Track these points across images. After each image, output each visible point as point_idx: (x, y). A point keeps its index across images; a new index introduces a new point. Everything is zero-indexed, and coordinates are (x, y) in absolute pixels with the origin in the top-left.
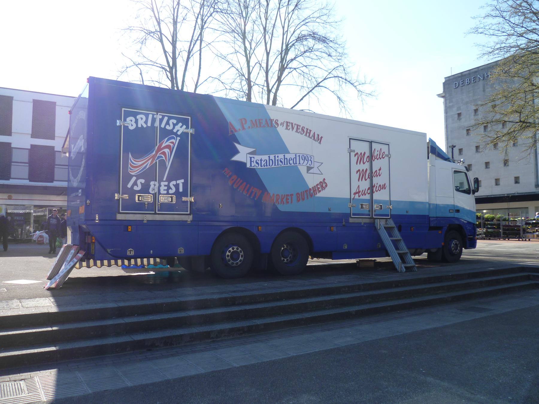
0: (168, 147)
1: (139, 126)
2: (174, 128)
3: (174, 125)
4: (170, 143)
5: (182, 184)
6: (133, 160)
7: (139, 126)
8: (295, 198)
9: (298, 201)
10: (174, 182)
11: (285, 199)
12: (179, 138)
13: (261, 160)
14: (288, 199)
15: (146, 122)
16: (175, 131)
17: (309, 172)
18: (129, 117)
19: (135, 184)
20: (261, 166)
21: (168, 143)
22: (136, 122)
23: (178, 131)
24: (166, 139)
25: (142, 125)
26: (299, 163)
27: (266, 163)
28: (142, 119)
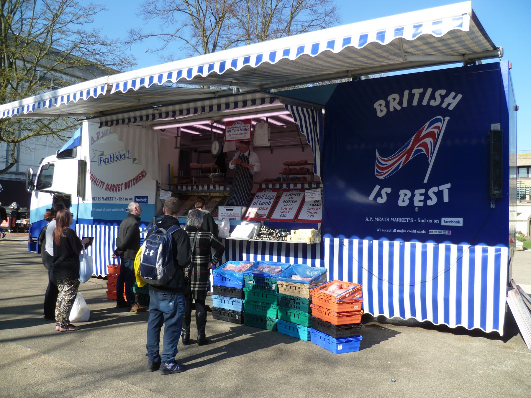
0: (431, 135)
1: (392, 109)
2: (442, 102)
3: (443, 97)
4: (433, 128)
5: (447, 190)
8: (123, 186)
9: (126, 188)
10: (435, 189)
11: (118, 187)
12: (447, 119)
13: (106, 159)
15: (400, 103)
16: (444, 106)
18: (378, 100)
19: (379, 194)
20: (106, 163)
21: (430, 130)
22: (387, 106)
23: (449, 104)
25: (394, 108)
26: (128, 157)
27: (109, 160)
28: (394, 99)
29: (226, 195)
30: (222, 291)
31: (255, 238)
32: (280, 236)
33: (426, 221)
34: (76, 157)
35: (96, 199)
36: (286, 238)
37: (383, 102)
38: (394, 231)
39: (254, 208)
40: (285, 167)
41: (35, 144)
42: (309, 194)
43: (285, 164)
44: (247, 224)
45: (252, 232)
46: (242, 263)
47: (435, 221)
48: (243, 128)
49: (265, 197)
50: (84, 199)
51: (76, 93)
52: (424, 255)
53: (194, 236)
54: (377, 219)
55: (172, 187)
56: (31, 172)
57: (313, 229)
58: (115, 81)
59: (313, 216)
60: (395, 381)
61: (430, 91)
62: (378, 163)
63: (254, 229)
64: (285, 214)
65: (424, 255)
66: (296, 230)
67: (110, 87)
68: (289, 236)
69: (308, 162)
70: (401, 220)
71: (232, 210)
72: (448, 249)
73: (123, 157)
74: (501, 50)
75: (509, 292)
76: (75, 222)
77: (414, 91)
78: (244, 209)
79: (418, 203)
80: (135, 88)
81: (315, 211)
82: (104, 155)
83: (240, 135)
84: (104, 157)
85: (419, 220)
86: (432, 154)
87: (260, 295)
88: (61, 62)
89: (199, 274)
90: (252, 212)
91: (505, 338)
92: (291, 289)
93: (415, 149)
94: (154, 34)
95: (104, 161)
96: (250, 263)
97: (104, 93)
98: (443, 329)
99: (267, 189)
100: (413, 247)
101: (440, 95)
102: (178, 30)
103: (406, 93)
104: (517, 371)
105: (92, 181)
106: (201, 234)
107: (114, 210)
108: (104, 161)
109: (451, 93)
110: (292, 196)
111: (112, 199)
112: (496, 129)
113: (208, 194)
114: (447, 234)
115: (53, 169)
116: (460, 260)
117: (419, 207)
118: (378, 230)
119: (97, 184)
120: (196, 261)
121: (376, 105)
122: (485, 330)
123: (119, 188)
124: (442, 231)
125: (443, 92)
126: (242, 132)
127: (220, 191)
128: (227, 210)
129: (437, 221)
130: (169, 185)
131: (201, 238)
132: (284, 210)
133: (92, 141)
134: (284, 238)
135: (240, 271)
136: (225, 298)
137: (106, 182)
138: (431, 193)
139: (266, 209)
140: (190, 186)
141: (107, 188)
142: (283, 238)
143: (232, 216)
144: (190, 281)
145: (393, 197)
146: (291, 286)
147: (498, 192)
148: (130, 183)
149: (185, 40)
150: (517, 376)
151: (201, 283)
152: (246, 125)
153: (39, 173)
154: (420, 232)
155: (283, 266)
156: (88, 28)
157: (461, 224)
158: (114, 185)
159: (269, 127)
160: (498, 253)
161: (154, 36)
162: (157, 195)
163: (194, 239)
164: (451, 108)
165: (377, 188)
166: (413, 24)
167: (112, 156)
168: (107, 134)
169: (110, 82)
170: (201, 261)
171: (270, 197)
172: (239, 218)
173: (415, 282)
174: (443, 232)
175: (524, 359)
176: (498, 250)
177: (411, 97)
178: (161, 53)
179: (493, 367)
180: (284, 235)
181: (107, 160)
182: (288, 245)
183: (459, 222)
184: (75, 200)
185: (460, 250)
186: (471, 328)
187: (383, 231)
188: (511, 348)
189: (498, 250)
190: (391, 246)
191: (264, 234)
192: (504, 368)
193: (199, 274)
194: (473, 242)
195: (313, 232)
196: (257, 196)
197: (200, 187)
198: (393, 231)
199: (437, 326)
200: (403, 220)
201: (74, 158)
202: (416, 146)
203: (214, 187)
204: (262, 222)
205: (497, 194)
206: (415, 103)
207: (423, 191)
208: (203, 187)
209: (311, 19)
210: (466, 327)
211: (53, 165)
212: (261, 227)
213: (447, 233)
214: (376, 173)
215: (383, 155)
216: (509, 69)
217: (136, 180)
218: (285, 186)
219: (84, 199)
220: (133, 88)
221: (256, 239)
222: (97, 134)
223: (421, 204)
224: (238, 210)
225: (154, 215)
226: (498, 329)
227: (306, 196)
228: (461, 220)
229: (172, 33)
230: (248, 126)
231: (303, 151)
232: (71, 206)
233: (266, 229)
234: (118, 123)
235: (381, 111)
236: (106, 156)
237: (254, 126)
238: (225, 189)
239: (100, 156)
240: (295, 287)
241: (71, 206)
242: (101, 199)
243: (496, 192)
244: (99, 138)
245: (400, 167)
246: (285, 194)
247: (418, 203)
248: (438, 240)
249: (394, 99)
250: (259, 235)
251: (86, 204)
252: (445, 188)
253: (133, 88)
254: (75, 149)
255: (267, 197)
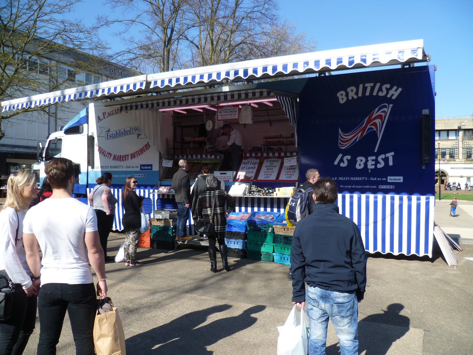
0: (380, 117)
1: (350, 98)
2: (387, 93)
3: (388, 90)
6: (343, 134)
7: (350, 98)
8: (130, 157)
9: (132, 158)
10: (383, 156)
11: (124, 157)
12: (391, 105)
13: (112, 134)
14: (126, 158)
15: (357, 93)
16: (389, 96)
17: (139, 138)
19: (341, 160)
20: (112, 138)
21: (379, 113)
22: (347, 95)
23: (393, 95)
24: (377, 109)
25: (352, 97)
26: (133, 133)
28: (352, 91)
29: (216, 162)
30: (228, 234)
31: (249, 195)
32: (268, 193)
33: (377, 179)
34: (83, 133)
35: (104, 167)
36: (273, 194)
37: (343, 93)
38: (354, 187)
39: (242, 172)
40: (265, 140)
41: (27, 121)
42: (287, 161)
43: (264, 138)
44: (239, 184)
45: (245, 190)
46: (241, 214)
47: (383, 179)
48: (233, 110)
49: (250, 163)
50: (93, 167)
51: (117, 87)
52: (376, 203)
53: (214, 194)
54: (341, 179)
55: (170, 156)
56: (41, 146)
57: (294, 187)
58: (153, 79)
59: (291, 177)
60: (369, 286)
61: (378, 85)
62: (341, 138)
63: (246, 188)
64: (268, 176)
65: (376, 203)
66: (280, 188)
67: (148, 83)
68: (275, 193)
69: (283, 136)
70: (358, 179)
71: (226, 174)
72: (392, 199)
73: (128, 133)
74: (429, 57)
75: (435, 227)
76: (86, 187)
77: (367, 85)
78: (235, 173)
79: (370, 166)
80: (171, 85)
81: (292, 173)
82: (110, 131)
83: (231, 116)
84: (110, 133)
85: (372, 179)
86: (380, 131)
87: (233, 243)
88: (44, 47)
89: (220, 221)
90: (241, 175)
91: (432, 260)
92: (284, 230)
93: (368, 127)
94: (119, 20)
95: (110, 136)
96: (248, 213)
97: (143, 88)
98: (389, 256)
99: (251, 156)
100: (368, 198)
101: (386, 88)
102: (139, 16)
103: (361, 86)
104: (445, 278)
105: (100, 153)
106: (209, 192)
107: (121, 176)
108: (110, 136)
109: (393, 87)
110: (272, 163)
111: (119, 167)
112: (425, 113)
113: (200, 161)
114: (392, 188)
115: (61, 143)
116: (401, 206)
117: (371, 169)
118: (341, 186)
119: (105, 155)
120: (217, 211)
121: (339, 95)
122: (419, 255)
123: (126, 158)
124: (388, 186)
125: (388, 86)
126: (232, 113)
127: (211, 159)
128: (221, 174)
129: (385, 179)
130: (168, 155)
131: (219, 194)
132: (267, 173)
133: (98, 120)
134: (271, 194)
135: (242, 219)
136: (231, 240)
137: (114, 153)
138: (380, 159)
139: (252, 172)
140: (186, 156)
141: (114, 158)
142: (270, 194)
143: (225, 179)
144: (214, 226)
145: (352, 162)
146: (284, 229)
147: (428, 158)
148: (136, 154)
149: (146, 25)
150: (445, 280)
151: (221, 227)
152: (234, 108)
153: (46, 146)
154: (372, 187)
155: (274, 215)
156: (69, 17)
157: (402, 181)
158: (121, 156)
159: (252, 109)
160: (428, 200)
161: (119, 22)
162: (160, 163)
163: (214, 196)
164: (394, 98)
165: (340, 156)
166: (385, 52)
167: (118, 132)
168: (112, 114)
169: (149, 80)
170: (220, 211)
171: (254, 164)
172: (231, 180)
173: (369, 223)
174: (388, 187)
175: (447, 271)
176: (428, 199)
177: (365, 89)
178: (123, 35)
179: (429, 276)
180: (271, 192)
181: (113, 136)
182: (272, 199)
183: (400, 179)
184: (84, 168)
185: (401, 199)
186: (409, 254)
187: (345, 187)
188: (437, 266)
189: (428, 199)
190: (351, 198)
191: (254, 191)
192: (435, 276)
193: (220, 221)
194: (410, 193)
195: (293, 188)
196: (243, 163)
197: (194, 156)
198: (353, 187)
199: (384, 255)
200: (360, 178)
201: (80, 133)
202: (369, 125)
203: (206, 156)
204: (251, 182)
205: (427, 159)
206: (368, 94)
207: (374, 158)
208: (197, 156)
209: (253, 6)
210: (406, 254)
211: (60, 140)
212: (250, 187)
213: (392, 187)
214: (339, 145)
215: (344, 132)
216: (435, 71)
217: (141, 152)
218: (265, 155)
219: (93, 167)
220: (170, 85)
221: (249, 196)
222: (103, 113)
223: (373, 167)
224: (230, 174)
225: (158, 179)
226: (428, 253)
227: (285, 162)
228: (401, 178)
229: (133, 19)
230: (236, 109)
231: (271, 126)
232: (81, 174)
233: (255, 188)
234: (137, 108)
235: (343, 99)
236: (113, 132)
237: (240, 109)
238: (216, 157)
239: (106, 132)
240: (288, 229)
241: (81, 174)
242: (109, 167)
243: (426, 158)
244: (105, 117)
245: (357, 140)
246: (266, 160)
247: (370, 166)
248: (386, 192)
249: (352, 91)
250: (250, 192)
251: (96, 172)
252: (390, 155)
253: (170, 85)
254: (81, 127)
255: (252, 163)
